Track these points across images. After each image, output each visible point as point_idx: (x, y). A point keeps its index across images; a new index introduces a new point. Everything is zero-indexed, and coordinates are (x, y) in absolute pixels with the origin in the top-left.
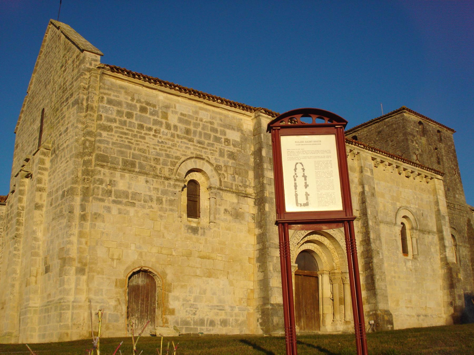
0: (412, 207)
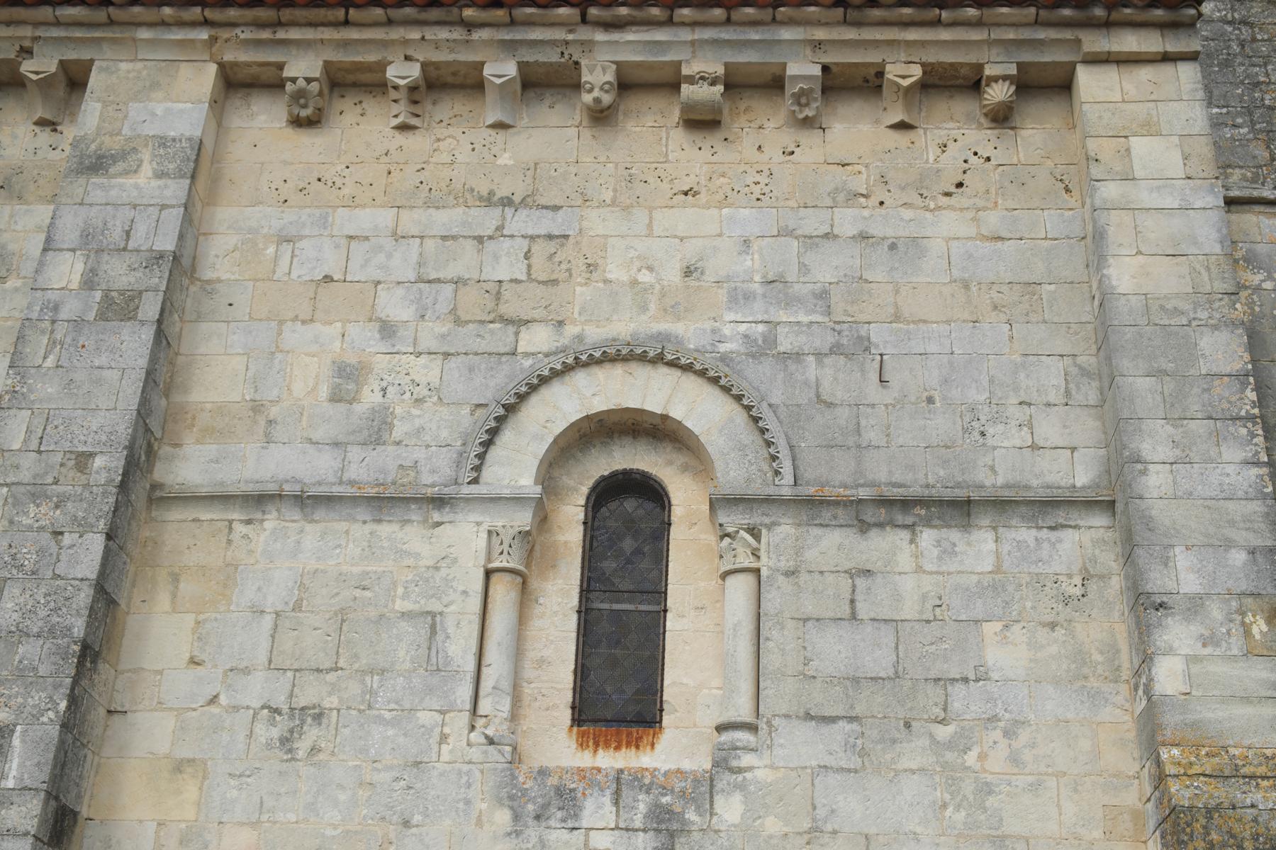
0: (727, 330)
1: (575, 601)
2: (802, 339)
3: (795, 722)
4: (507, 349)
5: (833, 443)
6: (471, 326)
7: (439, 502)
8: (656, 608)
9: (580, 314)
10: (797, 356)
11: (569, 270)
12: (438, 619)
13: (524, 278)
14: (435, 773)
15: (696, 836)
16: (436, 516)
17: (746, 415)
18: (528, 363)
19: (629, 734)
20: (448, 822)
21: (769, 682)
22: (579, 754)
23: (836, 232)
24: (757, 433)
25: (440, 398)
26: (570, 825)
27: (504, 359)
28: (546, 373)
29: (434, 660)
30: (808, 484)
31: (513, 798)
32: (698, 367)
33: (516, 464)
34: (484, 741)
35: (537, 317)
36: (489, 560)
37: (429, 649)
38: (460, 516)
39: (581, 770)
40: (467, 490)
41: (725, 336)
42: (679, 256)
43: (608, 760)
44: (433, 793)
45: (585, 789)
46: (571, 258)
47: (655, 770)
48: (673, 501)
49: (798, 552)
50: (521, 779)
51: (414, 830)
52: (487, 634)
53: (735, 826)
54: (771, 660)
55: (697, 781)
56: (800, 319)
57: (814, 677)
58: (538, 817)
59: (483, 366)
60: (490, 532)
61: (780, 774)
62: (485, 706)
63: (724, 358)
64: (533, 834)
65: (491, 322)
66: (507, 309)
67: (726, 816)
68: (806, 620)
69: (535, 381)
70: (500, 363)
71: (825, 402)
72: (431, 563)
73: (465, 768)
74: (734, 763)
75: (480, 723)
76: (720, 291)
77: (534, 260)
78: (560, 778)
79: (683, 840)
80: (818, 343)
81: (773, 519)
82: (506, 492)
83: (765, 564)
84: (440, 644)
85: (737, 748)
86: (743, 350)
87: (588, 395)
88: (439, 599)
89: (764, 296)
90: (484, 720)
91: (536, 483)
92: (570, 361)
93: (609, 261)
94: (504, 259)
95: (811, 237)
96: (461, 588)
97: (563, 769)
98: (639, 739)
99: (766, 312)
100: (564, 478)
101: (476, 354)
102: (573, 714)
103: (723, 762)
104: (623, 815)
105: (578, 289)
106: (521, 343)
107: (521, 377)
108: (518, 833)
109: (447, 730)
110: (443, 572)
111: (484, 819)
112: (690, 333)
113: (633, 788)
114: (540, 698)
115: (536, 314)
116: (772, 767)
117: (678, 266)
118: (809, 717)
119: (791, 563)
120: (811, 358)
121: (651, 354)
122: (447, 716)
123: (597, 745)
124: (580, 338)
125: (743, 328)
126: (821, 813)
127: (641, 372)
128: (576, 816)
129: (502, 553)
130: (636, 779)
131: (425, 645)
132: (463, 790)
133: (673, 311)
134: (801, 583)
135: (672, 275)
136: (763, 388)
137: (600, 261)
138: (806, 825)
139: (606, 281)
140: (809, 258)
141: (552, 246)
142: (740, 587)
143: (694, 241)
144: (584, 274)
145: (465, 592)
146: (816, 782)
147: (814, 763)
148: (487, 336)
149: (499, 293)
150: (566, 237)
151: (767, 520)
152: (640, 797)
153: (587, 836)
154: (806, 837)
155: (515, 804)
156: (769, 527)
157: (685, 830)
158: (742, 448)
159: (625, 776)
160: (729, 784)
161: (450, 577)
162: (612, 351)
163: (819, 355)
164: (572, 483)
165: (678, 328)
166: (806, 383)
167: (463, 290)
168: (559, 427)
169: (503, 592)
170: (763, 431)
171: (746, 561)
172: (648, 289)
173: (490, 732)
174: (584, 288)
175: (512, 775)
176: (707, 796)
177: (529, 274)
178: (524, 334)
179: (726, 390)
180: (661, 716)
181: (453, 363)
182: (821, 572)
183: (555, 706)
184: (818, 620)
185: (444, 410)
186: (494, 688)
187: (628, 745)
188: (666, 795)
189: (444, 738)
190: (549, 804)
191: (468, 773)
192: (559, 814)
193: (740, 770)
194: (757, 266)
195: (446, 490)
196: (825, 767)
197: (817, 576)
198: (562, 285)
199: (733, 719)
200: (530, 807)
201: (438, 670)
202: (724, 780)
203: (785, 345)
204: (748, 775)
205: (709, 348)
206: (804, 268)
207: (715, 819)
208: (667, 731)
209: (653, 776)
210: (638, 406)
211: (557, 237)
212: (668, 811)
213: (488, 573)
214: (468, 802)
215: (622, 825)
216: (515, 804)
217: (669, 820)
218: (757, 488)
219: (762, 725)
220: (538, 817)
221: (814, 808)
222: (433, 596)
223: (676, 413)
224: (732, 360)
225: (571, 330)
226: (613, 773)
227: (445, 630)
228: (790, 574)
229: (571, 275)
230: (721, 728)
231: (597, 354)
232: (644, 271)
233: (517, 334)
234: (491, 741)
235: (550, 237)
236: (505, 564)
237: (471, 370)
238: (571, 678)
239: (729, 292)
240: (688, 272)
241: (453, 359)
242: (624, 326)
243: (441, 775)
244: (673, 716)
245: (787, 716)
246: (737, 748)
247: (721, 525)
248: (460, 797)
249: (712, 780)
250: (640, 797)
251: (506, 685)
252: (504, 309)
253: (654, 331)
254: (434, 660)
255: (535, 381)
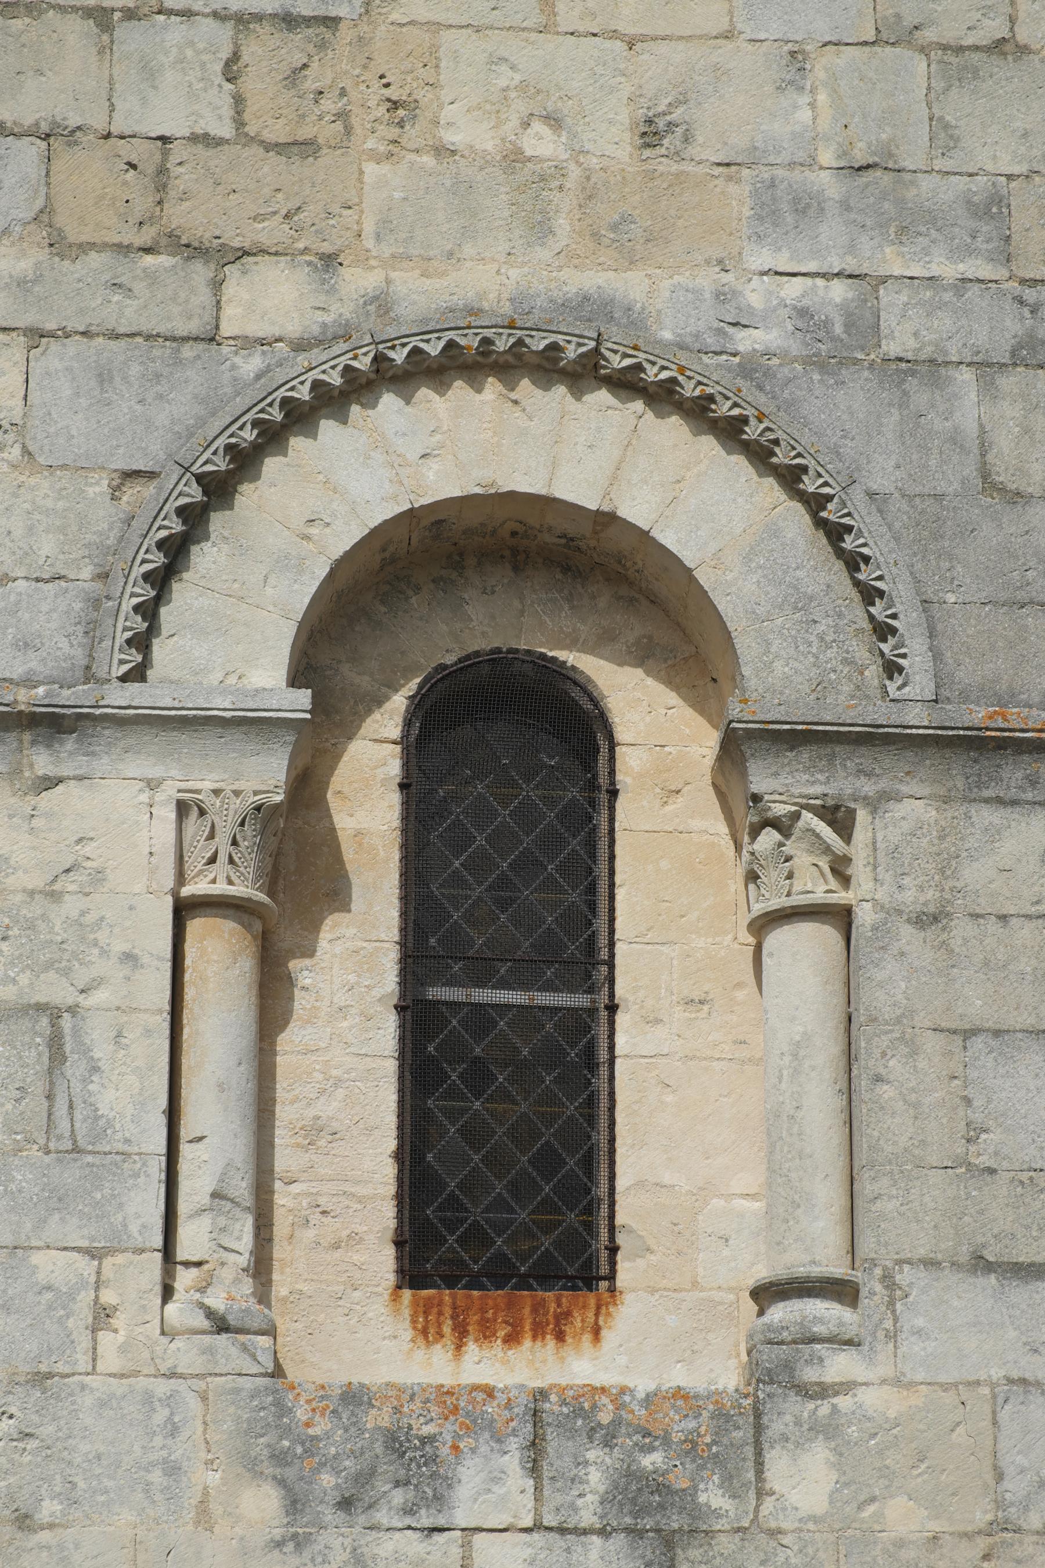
0: (755, 295)
1: (389, 982)
2: (944, 322)
3: (950, 1277)
4: (193, 327)
5: (1021, 595)
6: (94, 259)
7: (51, 724)
8: (579, 1000)
9: (378, 237)
10: (932, 368)
11: (342, 116)
12: (66, 1022)
13: (225, 130)
14: (88, 1400)
15: (726, 1544)
16: (42, 762)
17: (807, 519)
18: (251, 364)
19: (538, 1307)
20: (127, 1515)
21: (885, 1181)
22: (420, 1354)
23: (1023, 35)
24: (839, 565)
25: (26, 452)
26: (426, 1522)
27: (188, 351)
28: (304, 393)
29: (64, 1126)
30: (965, 697)
31: (283, 1457)
32: (689, 390)
33: (238, 630)
34: (206, 1324)
35: (265, 240)
36: (181, 878)
37: (50, 1097)
38: (102, 764)
39: (445, 1393)
40: (121, 697)
41: (750, 310)
42: (627, 90)
43: (503, 1368)
44: (84, 1447)
45: (457, 1436)
46: (346, 83)
47: (623, 1390)
48: (621, 734)
49: (947, 866)
50: (301, 1414)
51: (44, 1536)
52: (187, 1062)
53: (814, 1519)
54: (889, 1128)
55: (723, 1417)
56: (935, 270)
57: (992, 1171)
58: (346, 1504)
59: (135, 369)
60: (182, 808)
61: (917, 1399)
62: (192, 1239)
63: (750, 368)
64: (336, 1543)
65: (147, 250)
66: (195, 215)
67: (794, 1498)
68: (969, 1034)
69: (277, 415)
70: (178, 362)
71: (1002, 490)
72: (36, 881)
73: (162, 1387)
74: (810, 1374)
75: (184, 1278)
76: (732, 188)
77: (250, 84)
78: (397, 1410)
79: (695, 1553)
80: (981, 337)
81: (883, 784)
82: (221, 704)
83: (864, 895)
84: (76, 1087)
85: (813, 1340)
86: (795, 348)
87: (413, 456)
88: (66, 972)
89: (846, 206)
90: (194, 1272)
91: (295, 680)
92: (363, 364)
93: (446, 95)
94: (170, 77)
95: (960, 50)
96: (119, 947)
97: (401, 1389)
98: (563, 1317)
99: (851, 248)
100: (345, 669)
101: (115, 336)
102: (399, 1258)
103: (778, 1372)
104: (553, 1497)
105: (370, 168)
106: (229, 311)
107: (241, 403)
108: (300, 1542)
109: (108, 1297)
110: (72, 906)
111: (216, 1509)
112: (664, 301)
113: (573, 1433)
114: (315, 1218)
115: (270, 232)
116: (898, 1382)
117: (624, 117)
118: (981, 1264)
119: (930, 894)
120: (966, 375)
121: (571, 352)
122: (108, 1262)
123: (461, 1332)
124: (381, 303)
125: (793, 289)
126: (1015, 1487)
127: (546, 404)
128: (439, 1500)
129: (212, 860)
130: (579, 1412)
131: (39, 1088)
132: (158, 1441)
133: (619, 238)
134: (956, 944)
135: (611, 140)
136: (848, 448)
137: (425, 96)
138: (982, 1517)
139: (443, 151)
140: (957, 107)
141: (294, 48)
142: (802, 947)
143: (663, 48)
144: (383, 130)
145: (129, 958)
146: (1004, 1415)
147: (997, 1373)
148: (139, 287)
149: (162, 171)
150: (331, 22)
151: (868, 788)
152: (591, 1455)
153: (466, 1545)
154: (982, 1543)
155: (290, 1473)
156: (875, 804)
157: (699, 1529)
158: (801, 604)
159: (551, 1405)
160: (798, 1423)
161: (89, 919)
162: (470, 341)
163: (985, 367)
164: (364, 682)
165: (631, 286)
166: (955, 439)
167: (65, 160)
168: (343, 538)
169: (220, 957)
170: (853, 562)
171: (815, 886)
172: (548, 177)
173: (216, 1301)
174: (385, 168)
175: (278, 1404)
176: (749, 1451)
177: (239, 123)
178: (237, 287)
179: (760, 455)
180: (613, 1264)
181: (54, 358)
182: (1003, 918)
183: (354, 1239)
184: (997, 1033)
185: (42, 485)
186: (215, 1195)
187: (538, 1332)
188: (651, 1449)
189: (103, 1316)
190: (372, 1472)
191: (169, 1400)
192: (398, 1497)
193: (823, 1391)
194: (825, 123)
195: (66, 696)
196: (1023, 1381)
197: (992, 926)
198: (327, 157)
199: (801, 1271)
200: (327, 1480)
201: (76, 1150)
202: (788, 1413)
203: (900, 339)
204: (843, 1402)
205: (711, 341)
206: (943, 134)
207: (769, 1503)
208: (628, 1298)
209: (620, 1406)
210: (543, 492)
211: (309, 21)
212: (658, 1485)
213: (183, 911)
214: (173, 1470)
215: (549, 1520)
216: (290, 1473)
217: (661, 1506)
218: (845, 707)
219: (872, 1286)
220: (346, 1504)
221: (1000, 1477)
222: (49, 966)
223: (636, 510)
224: (768, 373)
225: (357, 281)
226: (523, 1399)
227: (85, 1051)
228: (929, 919)
229: (348, 130)
230: (766, 1294)
231: (434, 349)
232: (537, 126)
233: (217, 285)
234: (221, 1325)
235: (289, 21)
236: (221, 888)
237: (104, 378)
238: (390, 1170)
239: (755, 193)
240: (651, 134)
241: (55, 346)
242: (489, 277)
243: (102, 1404)
244: (640, 1263)
245: (930, 1263)
246: (813, 1340)
247: (756, 798)
248: (154, 1456)
249: (758, 1415)
250: (591, 1455)
251: (242, 1188)
252: (178, 215)
253: (571, 289)
254: (64, 1126)
255: (277, 415)
